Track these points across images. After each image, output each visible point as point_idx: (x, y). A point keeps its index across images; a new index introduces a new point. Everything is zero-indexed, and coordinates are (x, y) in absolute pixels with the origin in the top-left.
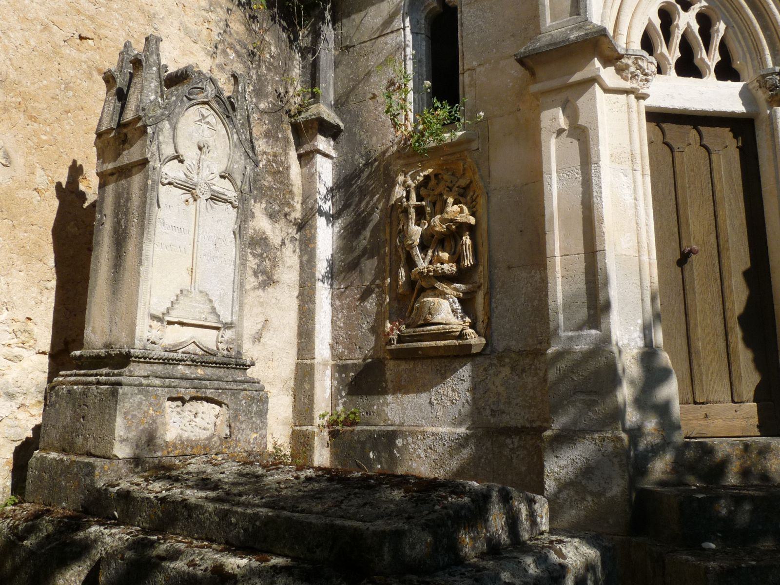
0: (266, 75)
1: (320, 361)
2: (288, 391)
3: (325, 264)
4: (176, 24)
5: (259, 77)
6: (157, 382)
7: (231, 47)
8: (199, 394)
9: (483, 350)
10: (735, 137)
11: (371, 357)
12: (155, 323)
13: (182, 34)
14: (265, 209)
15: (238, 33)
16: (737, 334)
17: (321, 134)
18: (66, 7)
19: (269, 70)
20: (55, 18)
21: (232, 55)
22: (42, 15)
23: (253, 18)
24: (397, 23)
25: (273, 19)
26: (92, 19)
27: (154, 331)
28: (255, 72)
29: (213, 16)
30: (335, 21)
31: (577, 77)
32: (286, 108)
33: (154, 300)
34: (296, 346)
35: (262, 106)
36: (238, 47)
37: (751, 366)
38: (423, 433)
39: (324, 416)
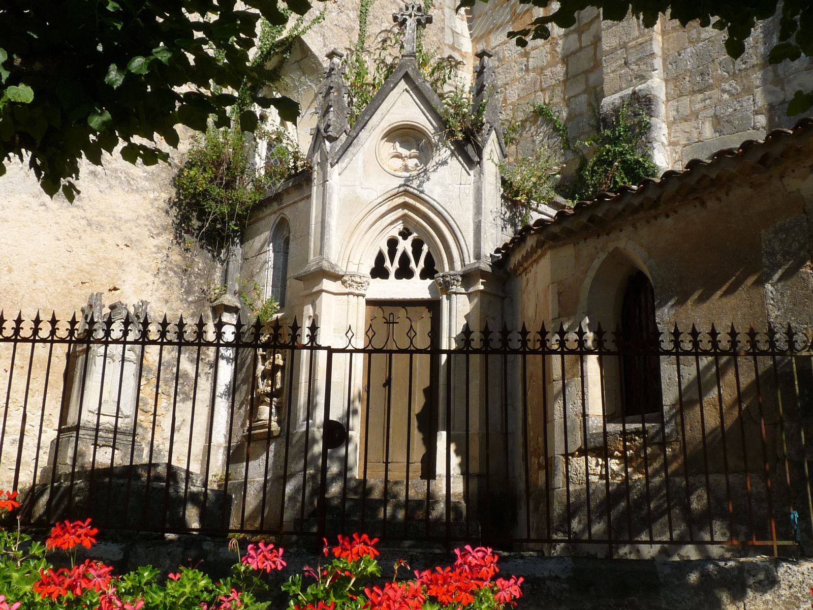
0: (194, 281)
1: (216, 444)
2: (197, 461)
3: (224, 387)
4: (136, 265)
5: (189, 284)
6: (88, 437)
7: (171, 269)
8: (107, 444)
9: (280, 434)
10: (429, 311)
11: (240, 441)
12: (91, 414)
13: (139, 270)
14: (188, 357)
15: (176, 261)
16: (415, 423)
17: (226, 312)
18: (76, 270)
19: (196, 278)
20: (70, 277)
21: (171, 274)
22: (63, 276)
23: (187, 250)
24: (265, 248)
25: (202, 247)
26: (88, 273)
27: (90, 417)
28: (186, 280)
29: (160, 255)
30: (242, 242)
31: (315, 289)
32: (208, 297)
33: (91, 405)
34: (205, 436)
35: (190, 299)
36: (176, 269)
37: (421, 442)
38: (254, 481)
39: (215, 476)
